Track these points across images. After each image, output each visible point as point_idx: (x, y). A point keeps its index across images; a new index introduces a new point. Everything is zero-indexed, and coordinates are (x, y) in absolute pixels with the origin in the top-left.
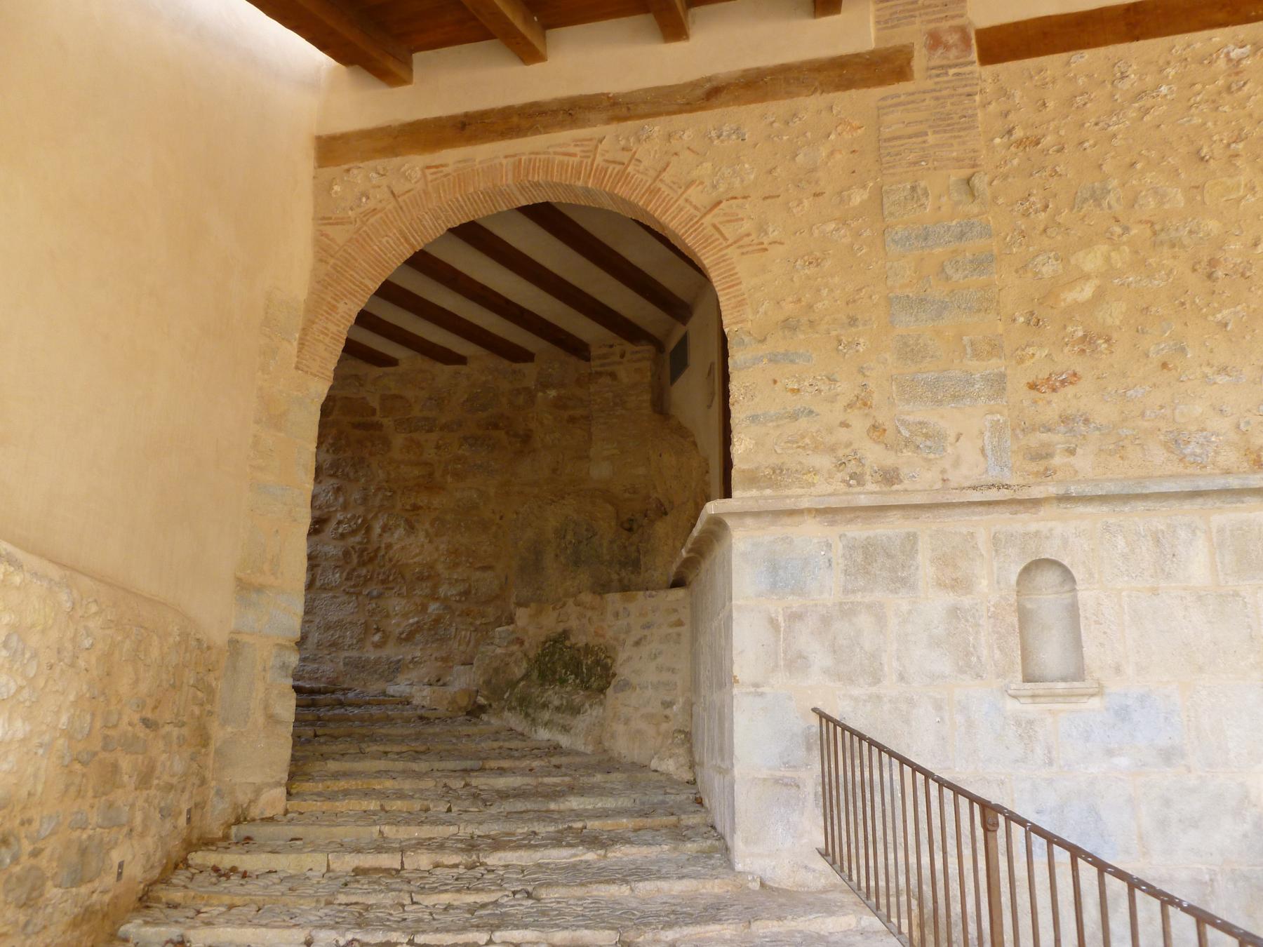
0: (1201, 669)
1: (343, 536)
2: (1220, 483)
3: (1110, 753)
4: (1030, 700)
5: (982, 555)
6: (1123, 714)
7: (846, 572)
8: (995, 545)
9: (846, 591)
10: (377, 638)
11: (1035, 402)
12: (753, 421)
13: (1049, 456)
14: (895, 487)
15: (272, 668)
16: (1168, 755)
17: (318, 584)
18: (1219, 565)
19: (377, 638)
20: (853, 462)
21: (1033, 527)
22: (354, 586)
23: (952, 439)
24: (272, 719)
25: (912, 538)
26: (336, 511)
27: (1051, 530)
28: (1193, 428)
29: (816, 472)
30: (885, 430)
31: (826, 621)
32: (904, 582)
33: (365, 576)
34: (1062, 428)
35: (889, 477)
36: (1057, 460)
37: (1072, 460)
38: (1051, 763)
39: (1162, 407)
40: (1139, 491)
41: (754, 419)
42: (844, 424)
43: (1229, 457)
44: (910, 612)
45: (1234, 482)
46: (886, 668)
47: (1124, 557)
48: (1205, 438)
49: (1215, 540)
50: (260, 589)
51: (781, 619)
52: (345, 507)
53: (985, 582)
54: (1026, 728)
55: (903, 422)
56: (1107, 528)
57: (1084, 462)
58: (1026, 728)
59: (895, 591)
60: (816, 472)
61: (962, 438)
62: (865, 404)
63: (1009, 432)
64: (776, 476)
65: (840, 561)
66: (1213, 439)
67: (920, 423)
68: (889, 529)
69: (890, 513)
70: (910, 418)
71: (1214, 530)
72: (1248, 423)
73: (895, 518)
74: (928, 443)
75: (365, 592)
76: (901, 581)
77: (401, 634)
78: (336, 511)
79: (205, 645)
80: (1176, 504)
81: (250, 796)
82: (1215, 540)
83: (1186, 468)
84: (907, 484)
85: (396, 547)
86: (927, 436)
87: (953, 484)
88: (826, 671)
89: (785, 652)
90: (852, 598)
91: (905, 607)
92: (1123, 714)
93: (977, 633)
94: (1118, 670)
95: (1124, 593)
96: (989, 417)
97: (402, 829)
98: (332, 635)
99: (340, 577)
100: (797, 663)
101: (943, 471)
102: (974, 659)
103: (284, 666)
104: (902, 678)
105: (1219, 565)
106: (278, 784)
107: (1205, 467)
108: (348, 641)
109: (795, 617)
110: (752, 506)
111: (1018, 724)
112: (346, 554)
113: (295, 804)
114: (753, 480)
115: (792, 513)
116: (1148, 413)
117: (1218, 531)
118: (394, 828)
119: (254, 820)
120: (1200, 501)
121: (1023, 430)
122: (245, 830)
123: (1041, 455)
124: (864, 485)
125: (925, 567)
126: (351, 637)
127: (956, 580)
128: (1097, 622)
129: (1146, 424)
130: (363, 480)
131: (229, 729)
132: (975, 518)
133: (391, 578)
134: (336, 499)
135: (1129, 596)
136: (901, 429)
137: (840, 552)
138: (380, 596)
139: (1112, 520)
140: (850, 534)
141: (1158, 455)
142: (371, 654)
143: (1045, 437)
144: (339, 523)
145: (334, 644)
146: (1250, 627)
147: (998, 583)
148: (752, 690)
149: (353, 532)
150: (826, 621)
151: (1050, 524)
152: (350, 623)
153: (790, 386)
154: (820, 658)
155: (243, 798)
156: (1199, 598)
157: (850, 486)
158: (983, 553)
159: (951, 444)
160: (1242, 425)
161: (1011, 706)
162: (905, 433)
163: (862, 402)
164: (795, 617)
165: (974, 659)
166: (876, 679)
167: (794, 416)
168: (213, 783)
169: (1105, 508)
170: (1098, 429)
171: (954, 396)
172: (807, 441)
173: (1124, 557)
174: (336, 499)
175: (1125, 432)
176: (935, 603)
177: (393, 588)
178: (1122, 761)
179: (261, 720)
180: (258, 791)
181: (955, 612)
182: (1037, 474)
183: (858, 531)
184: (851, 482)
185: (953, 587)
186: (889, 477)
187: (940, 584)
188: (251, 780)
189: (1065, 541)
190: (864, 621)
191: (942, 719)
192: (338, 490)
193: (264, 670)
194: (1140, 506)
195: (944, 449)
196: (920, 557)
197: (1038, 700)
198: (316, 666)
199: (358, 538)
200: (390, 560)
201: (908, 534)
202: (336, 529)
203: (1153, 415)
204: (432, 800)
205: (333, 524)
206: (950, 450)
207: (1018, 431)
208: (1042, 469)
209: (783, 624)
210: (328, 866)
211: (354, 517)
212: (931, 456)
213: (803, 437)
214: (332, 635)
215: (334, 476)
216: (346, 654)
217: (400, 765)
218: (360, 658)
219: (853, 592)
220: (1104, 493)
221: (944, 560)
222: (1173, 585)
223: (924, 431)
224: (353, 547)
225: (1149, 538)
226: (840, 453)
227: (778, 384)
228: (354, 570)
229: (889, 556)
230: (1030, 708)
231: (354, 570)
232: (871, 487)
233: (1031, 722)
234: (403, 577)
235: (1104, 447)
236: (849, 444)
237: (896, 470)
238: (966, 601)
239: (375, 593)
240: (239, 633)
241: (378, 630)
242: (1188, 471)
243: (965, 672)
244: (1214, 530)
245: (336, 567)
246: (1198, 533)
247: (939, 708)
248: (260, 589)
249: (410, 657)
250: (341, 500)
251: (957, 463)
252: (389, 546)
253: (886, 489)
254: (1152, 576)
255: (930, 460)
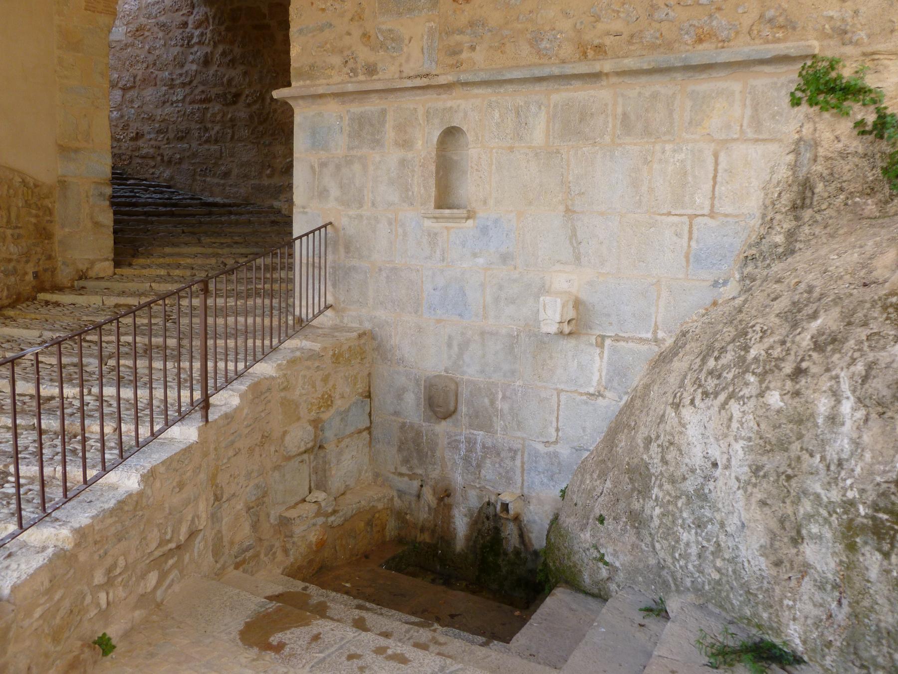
0: (530, 203)
1: (249, 105)
2: (556, 71)
3: (475, 255)
4: (435, 220)
5: (420, 124)
6: (484, 230)
7: (349, 136)
8: (427, 117)
9: (350, 148)
10: (268, 172)
11: (455, 11)
12: (300, 34)
13: (461, 52)
14: (375, 77)
15: (92, 196)
16: (505, 258)
17: (236, 137)
18: (551, 131)
19: (268, 172)
20: (352, 60)
21: (449, 104)
22: (257, 138)
23: (406, 41)
24: (97, 224)
25: (384, 112)
26: (245, 88)
27: (459, 106)
28: (547, 28)
29: (333, 68)
30: (370, 36)
31: (338, 167)
32: (378, 141)
33: (262, 132)
34: (469, 31)
35: (371, 70)
36: (464, 55)
37: (473, 54)
38: (443, 260)
39: (531, 12)
40: (500, 78)
41: (301, 31)
42: (349, 34)
43: (567, 50)
44: (380, 162)
45: (569, 70)
46: (366, 198)
47: (497, 124)
48: (553, 35)
49: (551, 112)
50: (77, 150)
51: (316, 166)
52: (250, 85)
53: (420, 143)
54: (433, 236)
55: (380, 30)
56: (490, 105)
57: (479, 56)
58: (433, 236)
59: (373, 149)
60: (333, 68)
61: (412, 41)
62: (360, 18)
63: (437, 35)
64: (311, 72)
65: (347, 128)
66: (559, 36)
67: (389, 30)
68: (372, 106)
69: (373, 95)
70: (384, 27)
71: (552, 106)
72: (582, 23)
73: (375, 98)
74: (394, 45)
75: (262, 142)
76: (377, 143)
77: (282, 169)
78: (245, 88)
79: (32, 184)
80: (643, 79)
81: (87, 265)
82: (551, 112)
83: (540, 58)
84: (380, 75)
85: (279, 111)
86: (393, 40)
87: (405, 75)
88: (337, 199)
89: (318, 187)
90: (353, 153)
91: (378, 159)
92: (484, 230)
93: (413, 176)
94: (485, 202)
95: (494, 151)
96: (427, 24)
97: (162, 285)
98: (244, 170)
99: (248, 132)
100: (323, 194)
101: (401, 65)
102: (410, 193)
103: (101, 194)
104: (373, 204)
105: (551, 131)
106: (107, 259)
107: (551, 58)
108: (253, 174)
109: (323, 165)
110: (305, 92)
111: (429, 235)
112: (251, 117)
113: (118, 270)
114: (301, 75)
115: (321, 96)
116: (521, 17)
117: (554, 106)
118: (158, 285)
119: (91, 278)
120: (545, 84)
121: (446, 33)
122: (82, 283)
123: (454, 52)
124: (357, 76)
125: (390, 134)
126: (255, 172)
127: (405, 141)
128: (477, 170)
129: (519, 26)
130: (259, 66)
131: (67, 230)
132: (417, 98)
133: (277, 132)
134: (244, 80)
135: (497, 153)
136: (379, 35)
137: (347, 122)
138: (270, 144)
139: (494, 99)
140: (352, 110)
141: (525, 49)
142: (266, 182)
143: (458, 38)
144: (247, 96)
145: (245, 176)
146: (562, 175)
147: (427, 143)
148: (302, 210)
149: (255, 102)
150: (338, 167)
151: (459, 102)
152: (254, 162)
153: (320, 7)
154: (335, 192)
155: (83, 267)
156: (536, 154)
157: (351, 77)
158: (421, 122)
159: (406, 45)
160: (578, 24)
161: (428, 223)
162: (381, 38)
163: (358, 17)
164: (323, 165)
165: (410, 193)
166: (361, 205)
167: (321, 29)
168: (60, 259)
169: (489, 90)
170: (490, 31)
171: (409, 9)
172: (328, 46)
173: (497, 124)
174: (244, 80)
175: (506, 32)
176: (393, 156)
177: (277, 139)
178: (481, 261)
179: (90, 225)
180: (92, 263)
181: (403, 163)
182: (452, 66)
183: (356, 108)
184: (351, 74)
185: (403, 146)
186: (371, 70)
187: (397, 144)
188: (86, 257)
189: (466, 114)
190: (357, 167)
191: (391, 230)
192: (245, 73)
193: (87, 197)
194: (510, 88)
195: (402, 50)
196: (387, 125)
197: (439, 220)
198: (236, 189)
199: (257, 106)
200: (276, 121)
201: (382, 109)
202: (245, 100)
203: (524, 18)
204: (198, 270)
205: (243, 97)
206: (405, 49)
207: (443, 34)
208: (455, 62)
209: (317, 170)
210: (103, 302)
211: (255, 91)
212: (395, 54)
213: (326, 43)
214: (244, 170)
215: (243, 63)
216: (253, 182)
217: (210, 251)
218: (260, 184)
219: (352, 149)
220: (479, 80)
221: (401, 128)
222: (523, 145)
223: (392, 36)
224: (255, 112)
225: (513, 111)
226: (346, 53)
227: (314, 5)
228: (256, 127)
229: (372, 125)
230: (436, 225)
231: (256, 127)
232: (361, 78)
233: (436, 234)
234: (283, 131)
235: (493, 45)
236: (350, 48)
237: (375, 65)
238: (410, 155)
239: (267, 142)
240: (65, 176)
241: (269, 166)
242: (541, 62)
243: (405, 202)
244: (552, 106)
245: (246, 126)
246: (543, 108)
247: (390, 224)
248: (77, 150)
249: (287, 183)
250: (247, 80)
251: (408, 60)
252: (275, 111)
253: (369, 79)
254: (511, 139)
255: (394, 57)
